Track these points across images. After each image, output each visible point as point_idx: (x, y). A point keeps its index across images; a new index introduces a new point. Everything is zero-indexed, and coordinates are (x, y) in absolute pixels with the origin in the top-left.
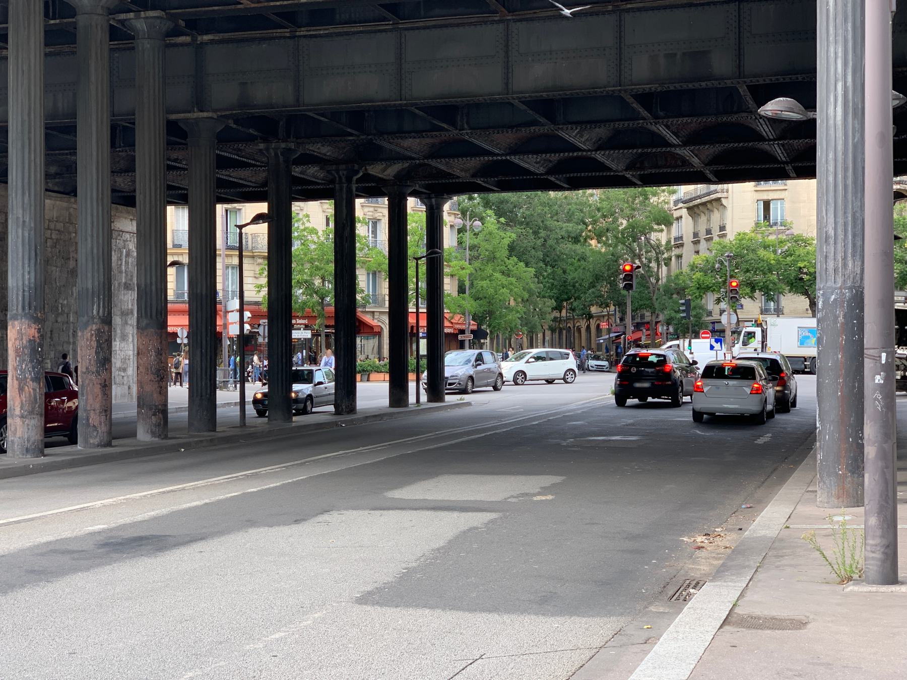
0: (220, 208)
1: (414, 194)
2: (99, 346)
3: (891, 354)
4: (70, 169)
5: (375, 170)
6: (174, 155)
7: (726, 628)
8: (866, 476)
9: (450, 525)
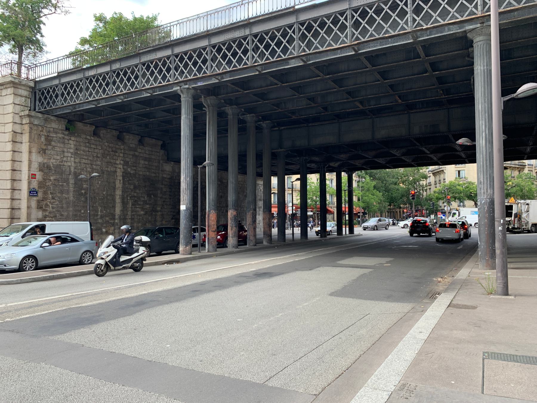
0: (286, 177)
1: (344, 171)
2: (253, 217)
3: (504, 220)
4: (245, 167)
5: (332, 164)
6: (273, 162)
7: (449, 308)
8: (497, 260)
9: (358, 272)
